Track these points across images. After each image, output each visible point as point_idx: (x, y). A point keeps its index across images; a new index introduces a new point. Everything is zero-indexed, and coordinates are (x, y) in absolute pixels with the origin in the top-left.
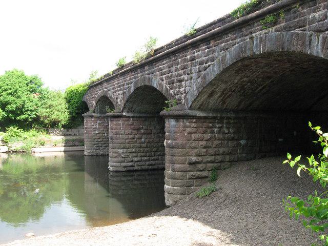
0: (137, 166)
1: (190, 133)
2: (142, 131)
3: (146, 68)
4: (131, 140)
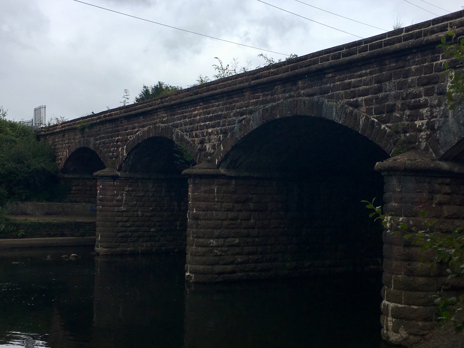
1: (440, 204)
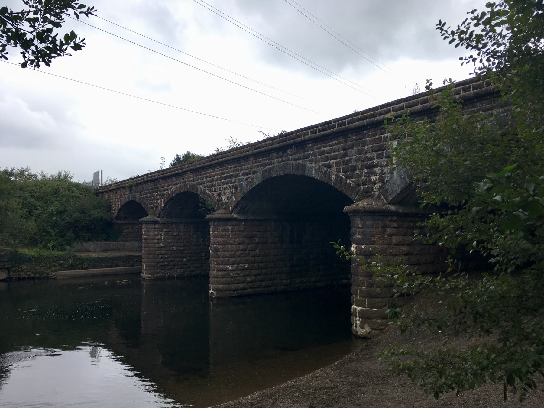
0: (251, 288)
1: (390, 235)
2: (257, 240)
4: (242, 252)
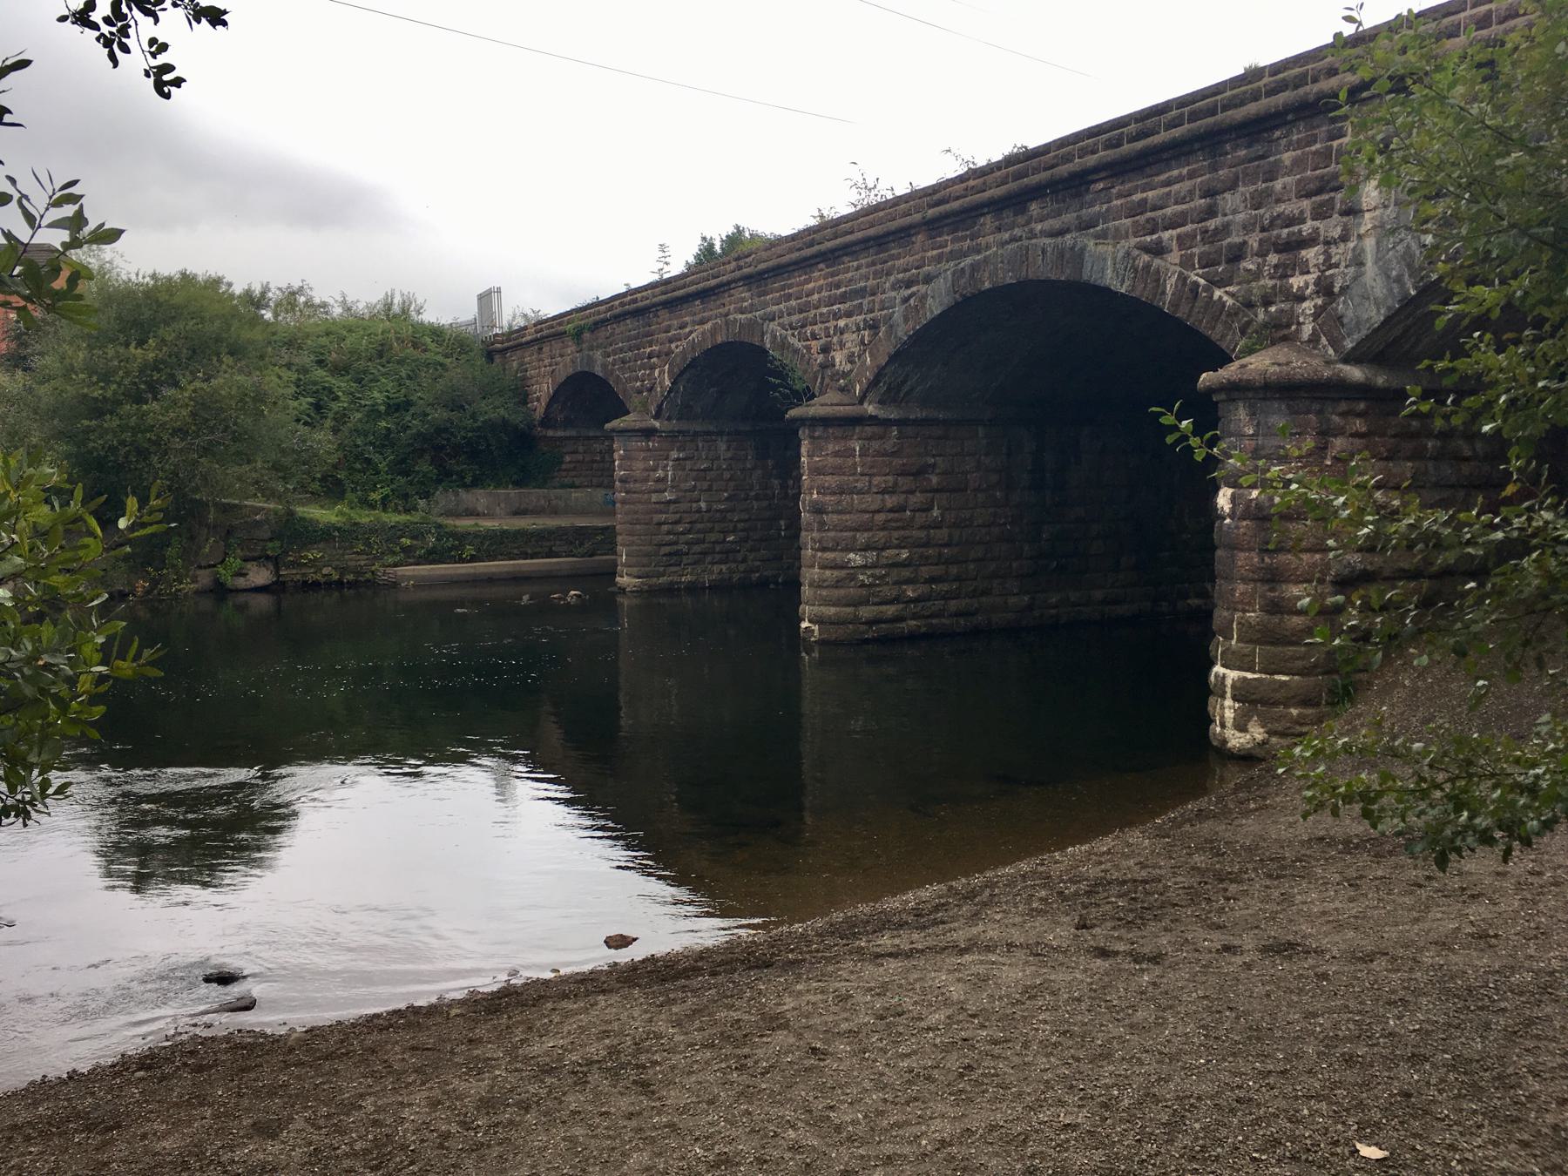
0: (915, 617)
3: (1034, 208)
4: (891, 516)
